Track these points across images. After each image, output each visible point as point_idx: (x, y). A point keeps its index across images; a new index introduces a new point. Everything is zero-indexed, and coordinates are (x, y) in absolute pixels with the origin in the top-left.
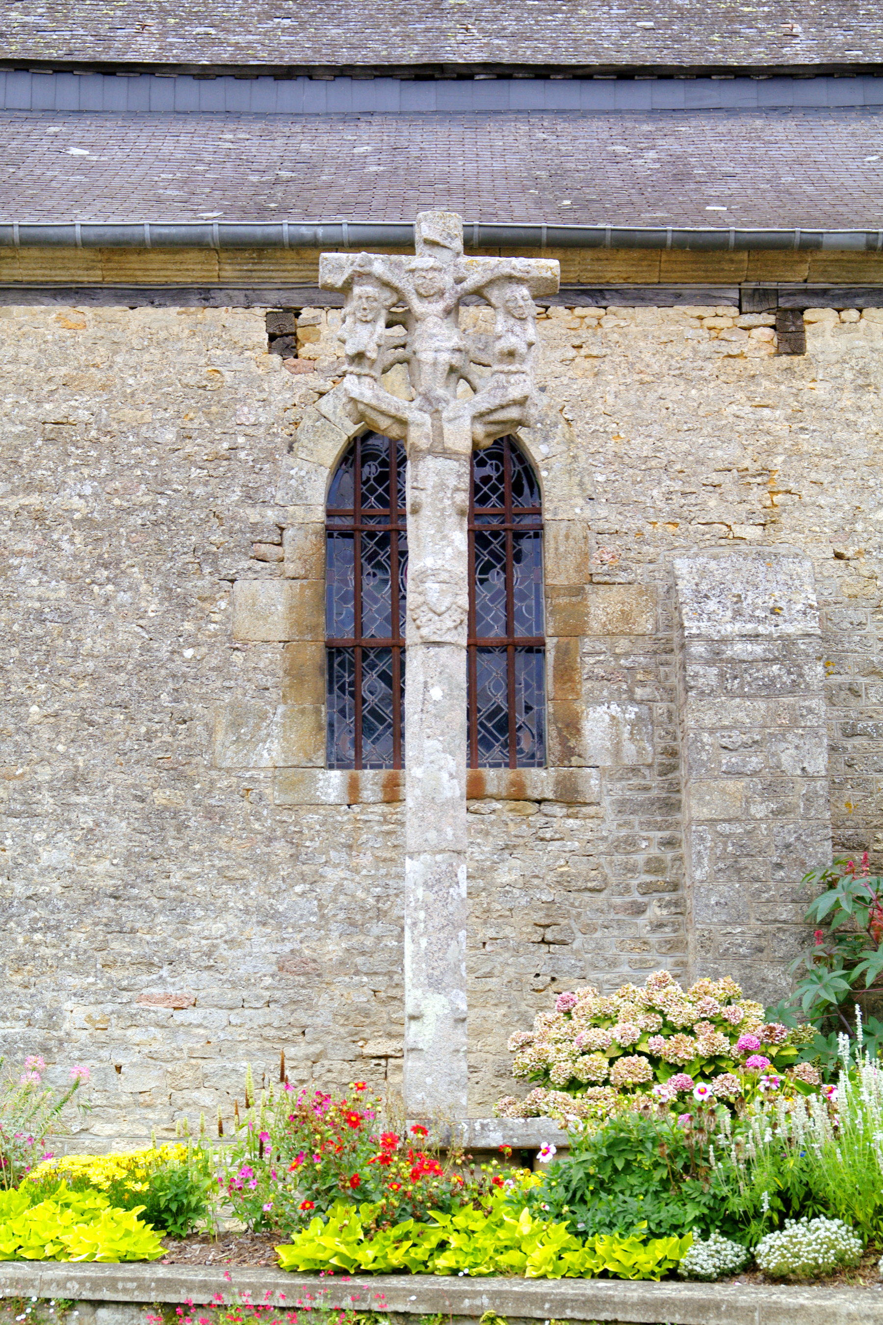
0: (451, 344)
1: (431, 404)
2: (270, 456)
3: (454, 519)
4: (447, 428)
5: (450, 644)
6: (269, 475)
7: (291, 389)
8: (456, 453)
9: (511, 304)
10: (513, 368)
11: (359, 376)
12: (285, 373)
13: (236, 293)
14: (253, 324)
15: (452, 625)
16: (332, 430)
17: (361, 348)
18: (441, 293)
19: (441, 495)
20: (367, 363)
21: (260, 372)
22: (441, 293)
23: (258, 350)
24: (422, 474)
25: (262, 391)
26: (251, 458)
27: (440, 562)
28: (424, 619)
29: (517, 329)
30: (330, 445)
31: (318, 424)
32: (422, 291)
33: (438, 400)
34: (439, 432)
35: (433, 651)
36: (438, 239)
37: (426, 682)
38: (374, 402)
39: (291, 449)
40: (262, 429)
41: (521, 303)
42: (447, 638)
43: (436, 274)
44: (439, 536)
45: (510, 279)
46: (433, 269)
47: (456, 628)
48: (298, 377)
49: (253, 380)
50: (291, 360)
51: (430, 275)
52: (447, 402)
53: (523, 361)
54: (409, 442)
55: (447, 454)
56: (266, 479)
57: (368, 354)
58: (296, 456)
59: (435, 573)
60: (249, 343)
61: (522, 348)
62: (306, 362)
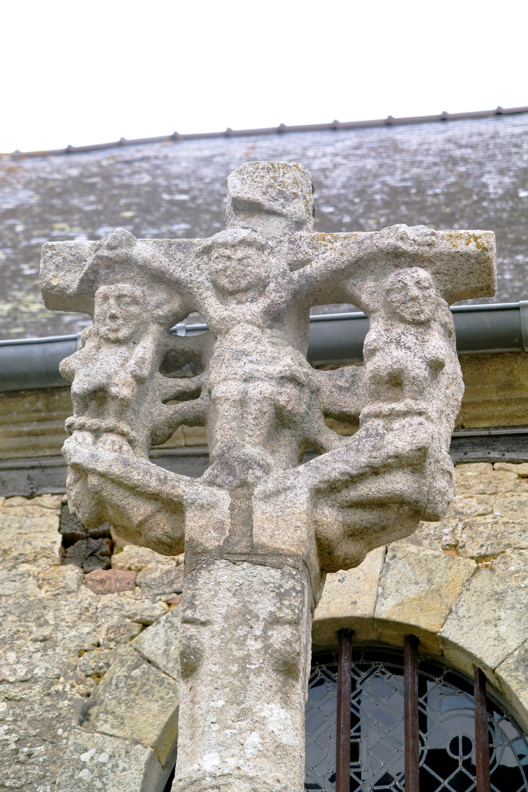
0: (276, 369)
1: (231, 472)
2: (47, 733)
3: (267, 679)
4: (261, 511)
6: (43, 765)
7: (94, 618)
8: (277, 553)
9: (396, 297)
10: (399, 406)
11: (97, 433)
12: (86, 593)
13: (14, 474)
14: (38, 520)
16: (161, 682)
17: (99, 379)
18: (259, 286)
19: (241, 632)
20: (112, 406)
21: (42, 594)
22: (259, 286)
23: (42, 562)
24: (204, 594)
25: (42, 623)
26: (14, 737)
27: (232, 762)
29: (410, 340)
30: (155, 707)
31: (136, 672)
32: (224, 282)
33: (248, 463)
34: (244, 518)
36: (257, 196)
38: (117, 470)
39: (85, 717)
40: (37, 688)
41: (415, 292)
43: (251, 251)
44: (233, 711)
45: (397, 257)
46: (244, 243)
48: (106, 599)
49: (30, 607)
50: (99, 573)
51: (240, 254)
52: (266, 469)
53: (420, 393)
54: (186, 538)
55: (257, 555)
56: (37, 771)
57: (114, 390)
58: (94, 730)
60: (28, 549)
61: (417, 369)
62: (121, 574)
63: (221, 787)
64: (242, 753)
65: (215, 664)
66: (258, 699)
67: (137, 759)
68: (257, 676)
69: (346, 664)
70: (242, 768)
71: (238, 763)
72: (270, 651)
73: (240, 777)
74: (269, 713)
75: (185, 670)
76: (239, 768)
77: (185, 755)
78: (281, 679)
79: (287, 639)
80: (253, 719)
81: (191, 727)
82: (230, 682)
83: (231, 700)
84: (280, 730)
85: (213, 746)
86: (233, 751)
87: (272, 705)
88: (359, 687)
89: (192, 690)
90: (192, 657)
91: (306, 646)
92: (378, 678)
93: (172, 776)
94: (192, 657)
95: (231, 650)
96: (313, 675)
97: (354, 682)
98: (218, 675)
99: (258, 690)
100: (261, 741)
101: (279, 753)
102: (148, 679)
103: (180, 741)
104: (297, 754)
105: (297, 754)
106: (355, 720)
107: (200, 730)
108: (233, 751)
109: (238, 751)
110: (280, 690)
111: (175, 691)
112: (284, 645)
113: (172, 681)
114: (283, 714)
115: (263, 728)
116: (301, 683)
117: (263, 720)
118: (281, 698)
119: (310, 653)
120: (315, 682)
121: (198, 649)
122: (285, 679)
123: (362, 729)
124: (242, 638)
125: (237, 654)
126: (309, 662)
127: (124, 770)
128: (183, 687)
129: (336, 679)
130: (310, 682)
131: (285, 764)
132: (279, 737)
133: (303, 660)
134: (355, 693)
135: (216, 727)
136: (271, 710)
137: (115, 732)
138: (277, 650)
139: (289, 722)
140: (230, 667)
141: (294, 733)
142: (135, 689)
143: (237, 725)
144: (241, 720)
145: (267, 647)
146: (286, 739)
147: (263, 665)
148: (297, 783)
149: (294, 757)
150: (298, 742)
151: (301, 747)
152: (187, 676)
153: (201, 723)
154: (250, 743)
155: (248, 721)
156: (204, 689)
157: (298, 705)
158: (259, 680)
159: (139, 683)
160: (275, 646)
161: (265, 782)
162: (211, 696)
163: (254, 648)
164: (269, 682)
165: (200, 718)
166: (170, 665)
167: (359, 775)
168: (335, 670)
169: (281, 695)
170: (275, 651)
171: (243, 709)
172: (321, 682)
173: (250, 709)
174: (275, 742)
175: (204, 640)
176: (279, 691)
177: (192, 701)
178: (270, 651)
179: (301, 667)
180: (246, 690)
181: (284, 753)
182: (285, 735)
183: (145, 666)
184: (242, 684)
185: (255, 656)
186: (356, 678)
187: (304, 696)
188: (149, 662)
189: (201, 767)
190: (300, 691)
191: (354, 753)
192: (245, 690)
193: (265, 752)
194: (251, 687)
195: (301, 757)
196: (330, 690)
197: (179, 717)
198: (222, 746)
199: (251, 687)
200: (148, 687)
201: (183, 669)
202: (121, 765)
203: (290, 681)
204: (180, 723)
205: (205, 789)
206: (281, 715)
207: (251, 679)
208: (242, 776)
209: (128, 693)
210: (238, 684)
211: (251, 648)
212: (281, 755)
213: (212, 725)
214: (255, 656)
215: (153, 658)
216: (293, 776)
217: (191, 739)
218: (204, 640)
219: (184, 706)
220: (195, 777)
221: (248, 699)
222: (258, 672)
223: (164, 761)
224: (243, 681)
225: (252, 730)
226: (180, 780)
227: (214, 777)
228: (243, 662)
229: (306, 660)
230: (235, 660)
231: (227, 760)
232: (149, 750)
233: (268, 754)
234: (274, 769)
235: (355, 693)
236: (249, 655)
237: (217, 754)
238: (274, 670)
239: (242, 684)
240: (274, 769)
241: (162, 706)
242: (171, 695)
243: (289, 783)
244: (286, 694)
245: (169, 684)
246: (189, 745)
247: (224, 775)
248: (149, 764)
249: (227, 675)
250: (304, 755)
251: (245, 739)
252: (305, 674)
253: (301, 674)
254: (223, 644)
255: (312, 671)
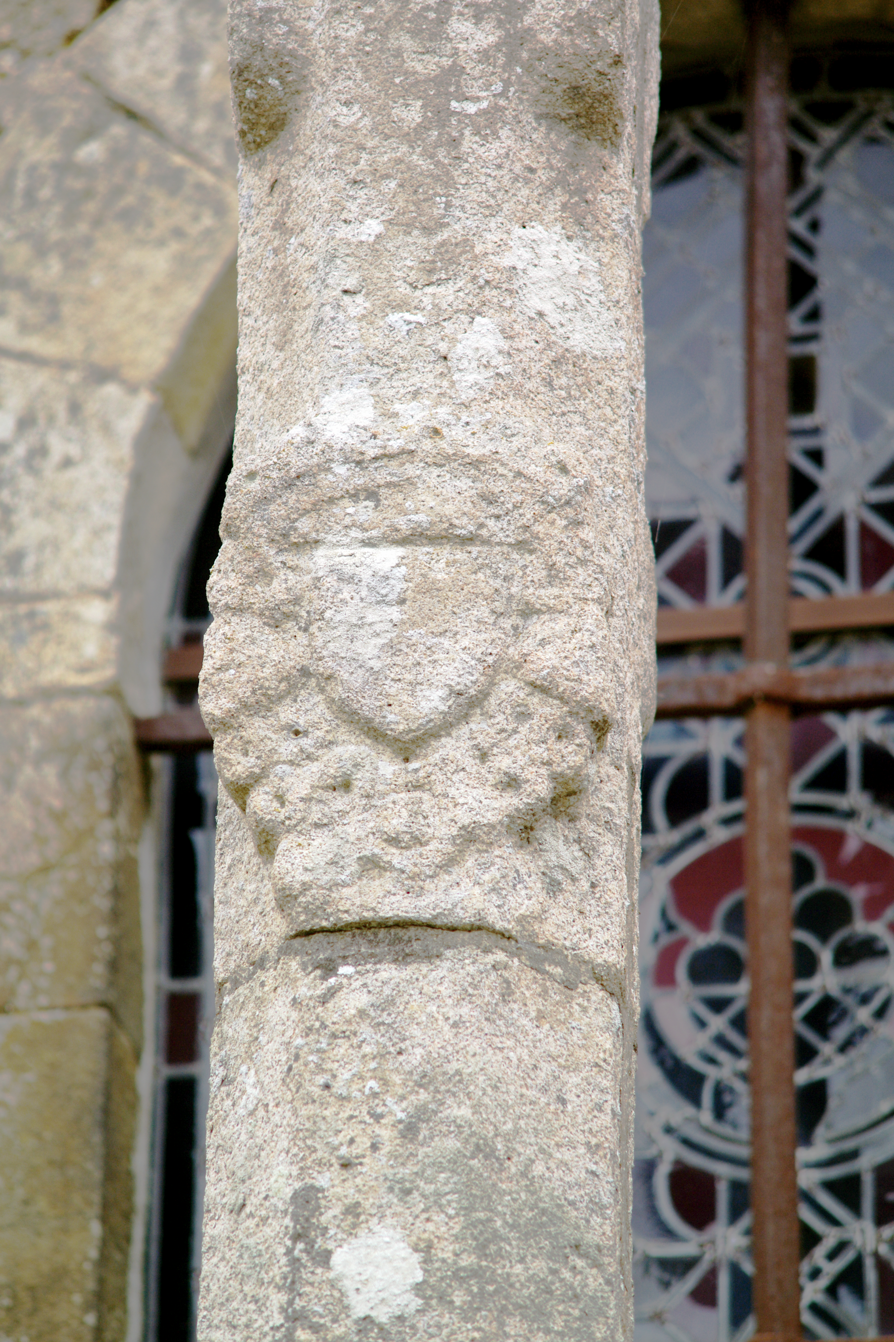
3: (511, 149)
5: (477, 928)
15: (496, 807)
16: (172, 181)
27: (414, 415)
28: (300, 782)
30: (158, 262)
31: (92, 151)
35: (359, 986)
37: (306, 1201)
42: (462, 894)
44: (411, 252)
47: (524, 830)
59: (376, 474)
63: (382, 491)
64: (445, 384)
65: (347, 103)
66: (492, 211)
67: (106, 428)
68: (485, 137)
69: (770, 104)
70: (445, 431)
71: (433, 416)
72: (525, 55)
73: (441, 461)
74: (527, 255)
75: (253, 126)
76: (436, 432)
77: (261, 396)
78: (562, 146)
79: (580, 12)
80: (475, 278)
81: (279, 308)
82: (399, 161)
83: (404, 219)
84: (563, 308)
85: (352, 365)
86: (416, 379)
87: (536, 231)
88: (813, 176)
89: (278, 189)
90: (273, 82)
91: (640, 35)
92: (876, 149)
93: (227, 466)
94: (273, 82)
95: (398, 53)
96: (664, 144)
97: (796, 161)
98: (359, 138)
99: (491, 183)
100: (505, 345)
101: (564, 381)
102: (131, 173)
103: (244, 353)
104: (618, 384)
105: (618, 384)
106: (800, 283)
107: (309, 318)
108: (416, 379)
109: (430, 379)
110: (560, 181)
111: (221, 209)
112: (570, 31)
113: (207, 178)
114: (572, 256)
115: (508, 303)
116: (627, 155)
117: (510, 280)
118: (564, 207)
119: (656, 56)
120: (671, 168)
121: (292, 54)
122: (576, 144)
123: (827, 311)
124: (432, 15)
125: (419, 67)
126: (654, 87)
127: (67, 463)
128: (249, 184)
129: (740, 154)
130: (656, 164)
131: (583, 415)
132: (561, 331)
133: (631, 81)
134: (801, 196)
135: (358, 305)
136: (533, 245)
137: (34, 343)
138: (546, 50)
139: (592, 283)
140: (398, 112)
141: (608, 317)
142: (91, 207)
143: (426, 296)
144: (439, 283)
145: (515, 41)
146: (581, 338)
147: (502, 102)
148: (623, 472)
149: (611, 392)
150: (623, 345)
151: (631, 361)
152: (259, 146)
153: (311, 295)
154: (470, 352)
155: (460, 284)
156: (316, 186)
157: (618, 228)
158: (494, 150)
159: (102, 187)
160: (542, 36)
161: (519, 474)
162: (338, 206)
163: (473, 46)
164: (526, 155)
165: (306, 278)
166: (202, 125)
167: (816, 456)
168: (734, 123)
169: (564, 198)
170: (543, 53)
171: (443, 244)
172: (690, 167)
173: (466, 244)
174: (549, 346)
175: (310, 26)
176: (556, 182)
177: (279, 226)
178: (525, 55)
179: (625, 103)
180: (449, 183)
181: (580, 380)
182: (579, 325)
183: (119, 129)
184: (438, 164)
185: (476, 73)
186: (803, 146)
187: (639, 198)
188: (132, 115)
189: (315, 431)
190: (624, 183)
191: (802, 387)
192: (447, 185)
193: (518, 378)
194: (468, 173)
195: (633, 391)
196: (720, 191)
197: (240, 279)
198: (382, 364)
199: (468, 173)
200: (129, 200)
201: (247, 121)
202: (58, 447)
203: (593, 148)
204: (242, 297)
205: (332, 500)
206: (565, 260)
207: (465, 147)
208: (448, 458)
209: (69, 218)
210: (424, 164)
211: (462, 46)
212: (568, 388)
213: (347, 299)
214: (476, 73)
215: (141, 102)
216: (610, 451)
217: (280, 347)
218: (310, 26)
219: (253, 241)
220: (297, 463)
221: (457, 213)
222: (488, 123)
223: (193, 429)
224: (441, 154)
225: (473, 313)
226: (251, 475)
227: (358, 463)
228: (438, 94)
229: (644, 81)
230: (413, 87)
231: (397, 407)
232: (143, 402)
233: (529, 385)
234: (547, 431)
235: (801, 196)
236: (456, 71)
237: (365, 390)
238: (538, 117)
239: (438, 164)
240: (547, 431)
241: (181, 260)
242: (207, 221)
243: (596, 475)
244: (580, 191)
245: (199, 186)
246: (276, 364)
247: (391, 457)
248: (147, 441)
249: (387, 137)
250: (641, 386)
251: (454, 341)
252: (640, 128)
253: (628, 128)
254: (372, 36)
255: (662, 132)
